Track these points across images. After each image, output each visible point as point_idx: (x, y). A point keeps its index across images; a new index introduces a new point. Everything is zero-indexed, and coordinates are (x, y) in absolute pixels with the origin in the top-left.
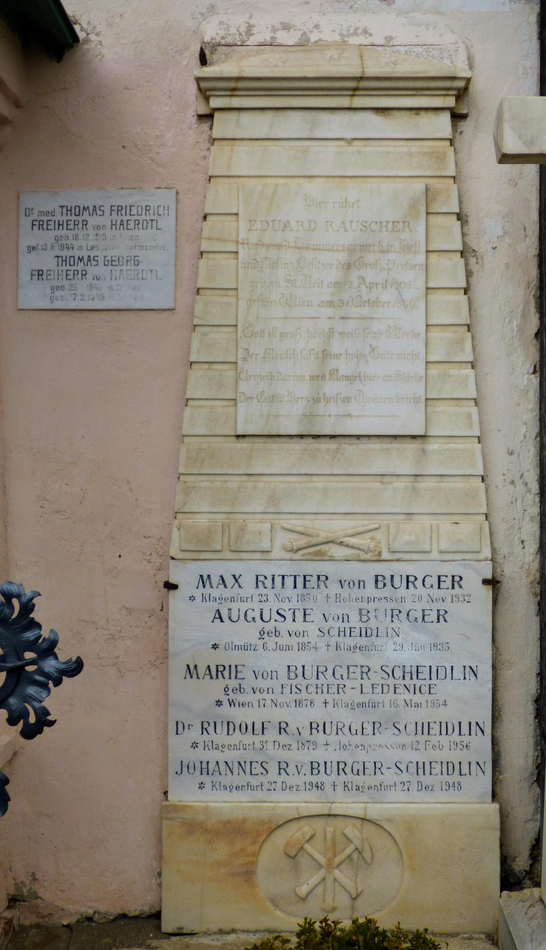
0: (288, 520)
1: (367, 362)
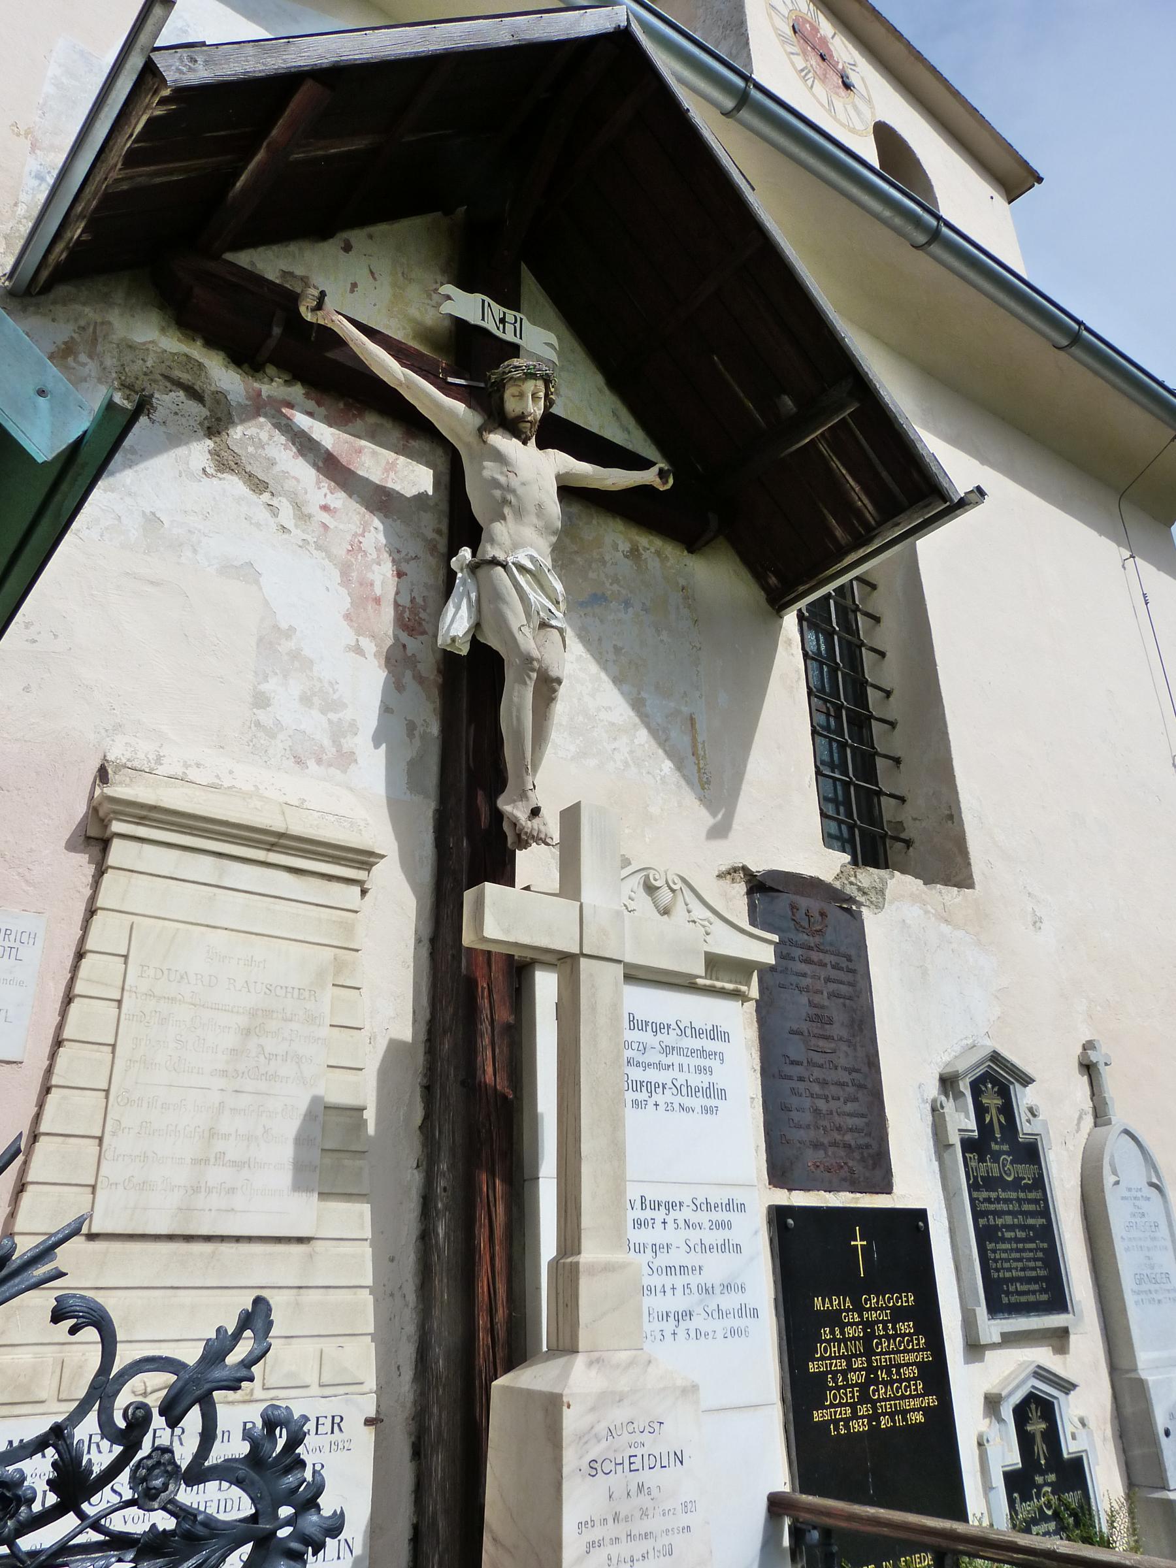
0: (142, 1350)
1: (258, 1145)
